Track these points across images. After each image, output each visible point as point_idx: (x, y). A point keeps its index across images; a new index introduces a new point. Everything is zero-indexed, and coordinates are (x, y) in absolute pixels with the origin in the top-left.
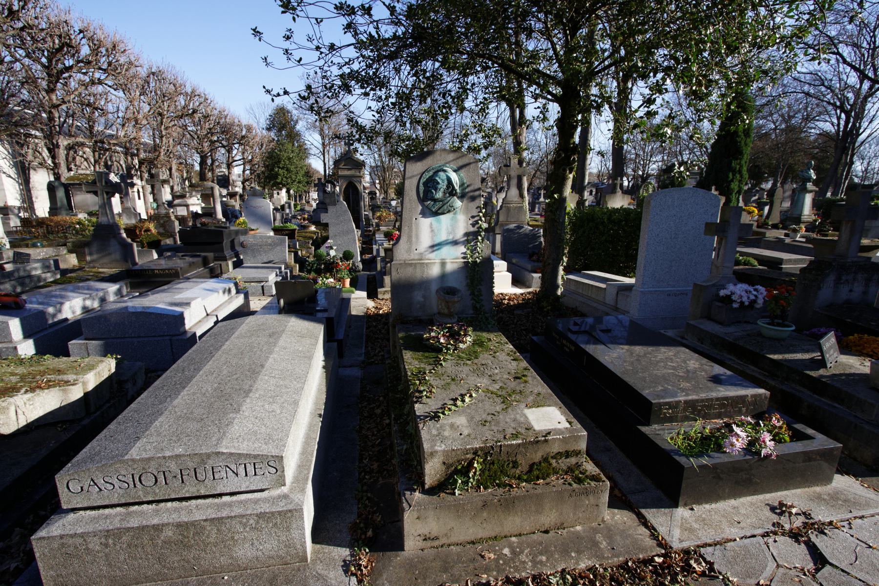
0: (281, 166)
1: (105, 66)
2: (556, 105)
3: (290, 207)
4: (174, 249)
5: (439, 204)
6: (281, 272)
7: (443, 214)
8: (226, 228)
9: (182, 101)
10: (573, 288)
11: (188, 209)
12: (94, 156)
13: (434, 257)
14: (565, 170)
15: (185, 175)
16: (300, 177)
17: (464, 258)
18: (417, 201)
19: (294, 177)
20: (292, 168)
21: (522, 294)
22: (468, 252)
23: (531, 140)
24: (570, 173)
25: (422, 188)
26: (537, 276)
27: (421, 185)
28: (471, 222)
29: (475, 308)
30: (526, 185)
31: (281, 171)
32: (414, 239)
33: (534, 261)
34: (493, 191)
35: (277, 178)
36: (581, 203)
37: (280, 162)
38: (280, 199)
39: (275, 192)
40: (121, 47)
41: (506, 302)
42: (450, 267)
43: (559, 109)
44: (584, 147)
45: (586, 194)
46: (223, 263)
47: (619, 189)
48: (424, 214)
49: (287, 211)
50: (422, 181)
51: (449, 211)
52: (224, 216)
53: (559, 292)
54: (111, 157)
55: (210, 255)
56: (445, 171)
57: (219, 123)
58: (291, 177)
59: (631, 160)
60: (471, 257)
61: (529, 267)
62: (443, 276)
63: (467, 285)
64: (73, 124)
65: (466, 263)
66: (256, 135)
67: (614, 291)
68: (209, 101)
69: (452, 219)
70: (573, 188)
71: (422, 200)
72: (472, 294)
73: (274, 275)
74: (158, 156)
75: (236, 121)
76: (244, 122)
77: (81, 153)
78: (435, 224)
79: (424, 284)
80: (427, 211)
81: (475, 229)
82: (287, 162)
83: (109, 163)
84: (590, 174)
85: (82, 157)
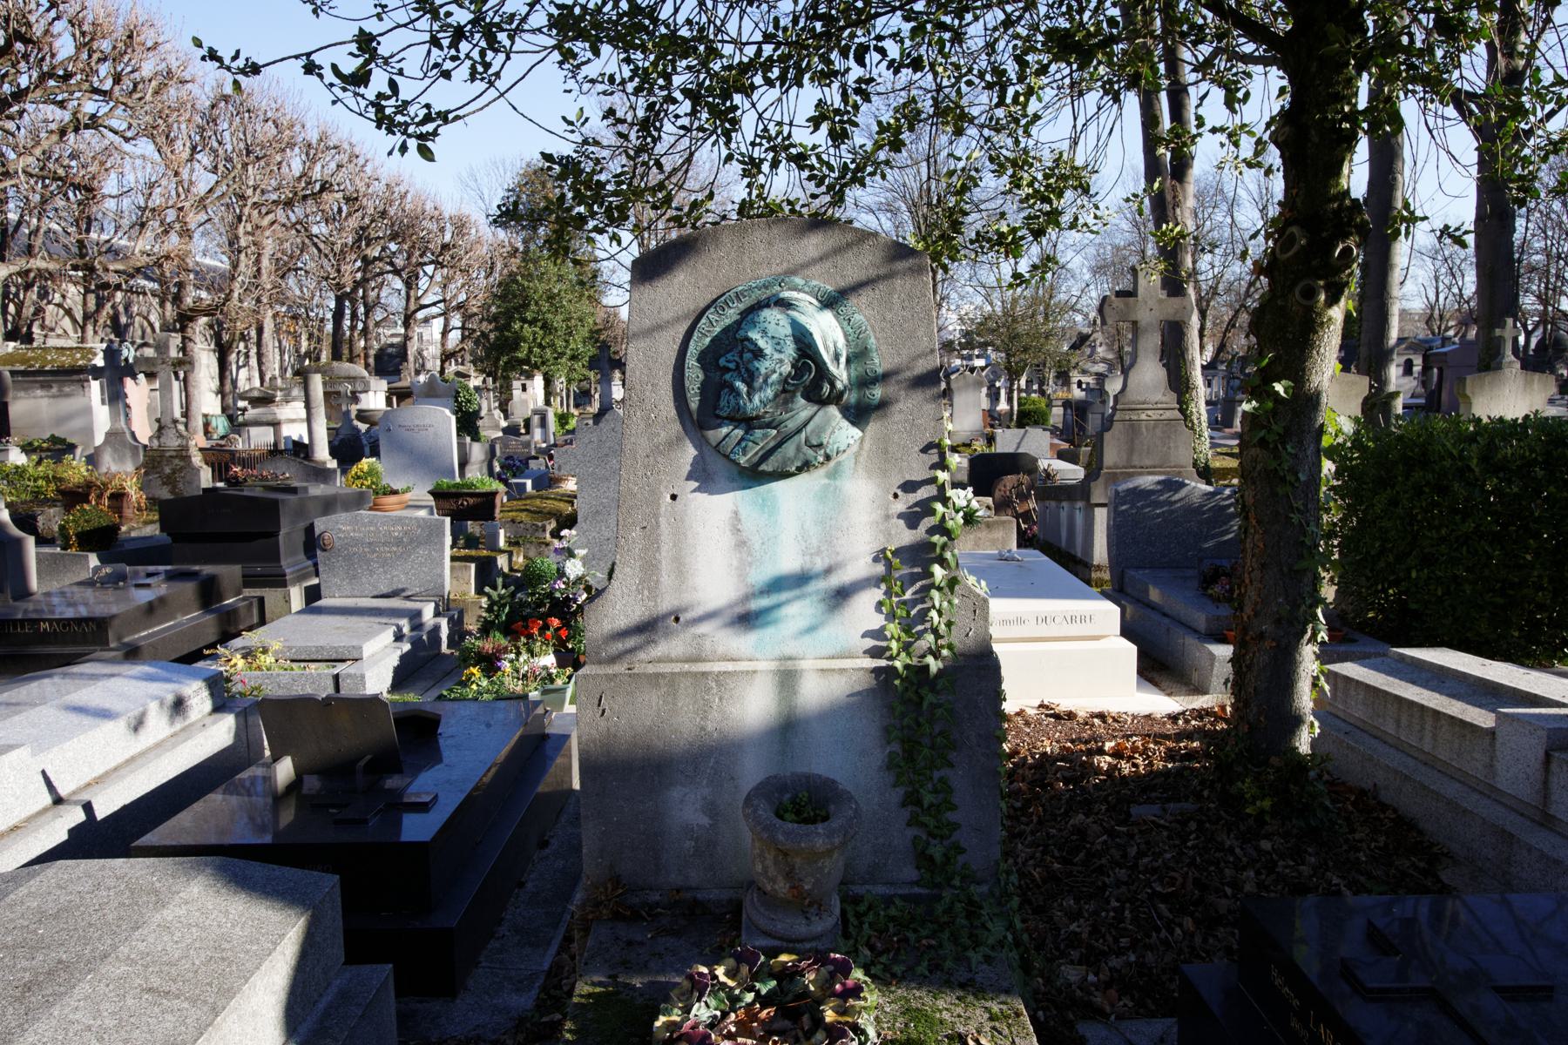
0: (529, 315)
1: (107, 85)
2: (1276, 78)
3: (543, 423)
4: (145, 554)
5: (764, 438)
7: (784, 475)
8: (294, 491)
10: (1358, 712)
11: (277, 434)
12: (85, 303)
14: (1311, 294)
15: (304, 345)
17: (875, 653)
19: (560, 343)
20: (557, 321)
21: (1174, 718)
22: (893, 629)
23: (1220, 226)
24: (1333, 300)
25: (694, 374)
26: (1224, 651)
28: (900, 507)
29: (923, 859)
30: (1198, 356)
33: (1216, 600)
34: (1111, 367)
35: (517, 347)
36: (1376, 403)
37: (525, 306)
39: (517, 384)
40: (148, 37)
41: (1104, 762)
42: (815, 692)
44: (1384, 217)
45: (1394, 372)
46: (271, 596)
47: (1509, 355)
48: (703, 476)
49: (537, 434)
50: (693, 349)
51: (806, 466)
53: (1304, 743)
54: (127, 308)
55: (229, 573)
56: (785, 305)
57: (384, 214)
58: (552, 345)
59: (1533, 269)
60: (906, 647)
61: (1200, 619)
62: (788, 729)
63: (890, 764)
64: (38, 229)
65: (884, 676)
67: (1533, 749)
68: (361, 161)
69: (824, 496)
70: (1346, 363)
72: (912, 799)
74: (227, 299)
75: (429, 206)
76: (449, 210)
77: (57, 298)
79: (710, 758)
80: (717, 464)
81: (920, 533)
82: (546, 306)
83: (123, 320)
84: (1403, 312)
85: (59, 305)
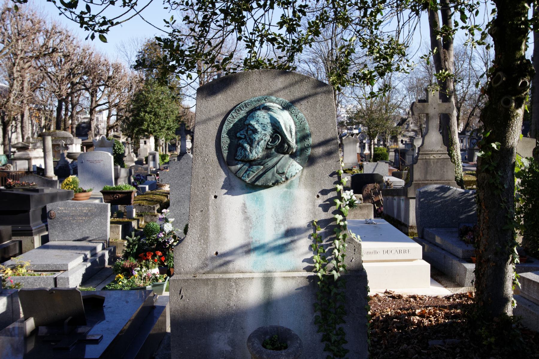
0: (148, 109)
3: (154, 159)
5: (257, 170)
6: (94, 254)
7: (266, 187)
8: (37, 191)
9: (41, 40)
11: (29, 164)
13: (249, 266)
14: (508, 103)
15: (43, 123)
16: (170, 122)
17: (309, 269)
18: (217, 164)
19: (162, 122)
20: (161, 112)
21: (448, 298)
22: (317, 258)
24: (518, 106)
25: (225, 140)
26: (471, 267)
27: (224, 135)
28: (320, 201)
30: (457, 129)
31: (147, 116)
32: (212, 235)
33: (467, 242)
35: (142, 124)
37: (146, 105)
38: (146, 149)
39: (142, 141)
41: (416, 319)
42: (281, 287)
43: (494, 7)
46: (25, 240)
48: (230, 188)
49: (151, 164)
50: (225, 129)
51: (277, 183)
52: (56, 173)
53: (509, 311)
56: (267, 109)
57: (81, 63)
58: (158, 123)
60: (323, 267)
61: (460, 252)
62: (268, 305)
65: (313, 279)
66: (125, 75)
68: (71, 39)
69: (284, 196)
71: (226, 163)
72: (326, 338)
73: (80, 259)
74: (7, 101)
75: (102, 59)
76: (111, 61)
78: (252, 207)
79: (232, 318)
80: (235, 182)
82: (156, 105)
